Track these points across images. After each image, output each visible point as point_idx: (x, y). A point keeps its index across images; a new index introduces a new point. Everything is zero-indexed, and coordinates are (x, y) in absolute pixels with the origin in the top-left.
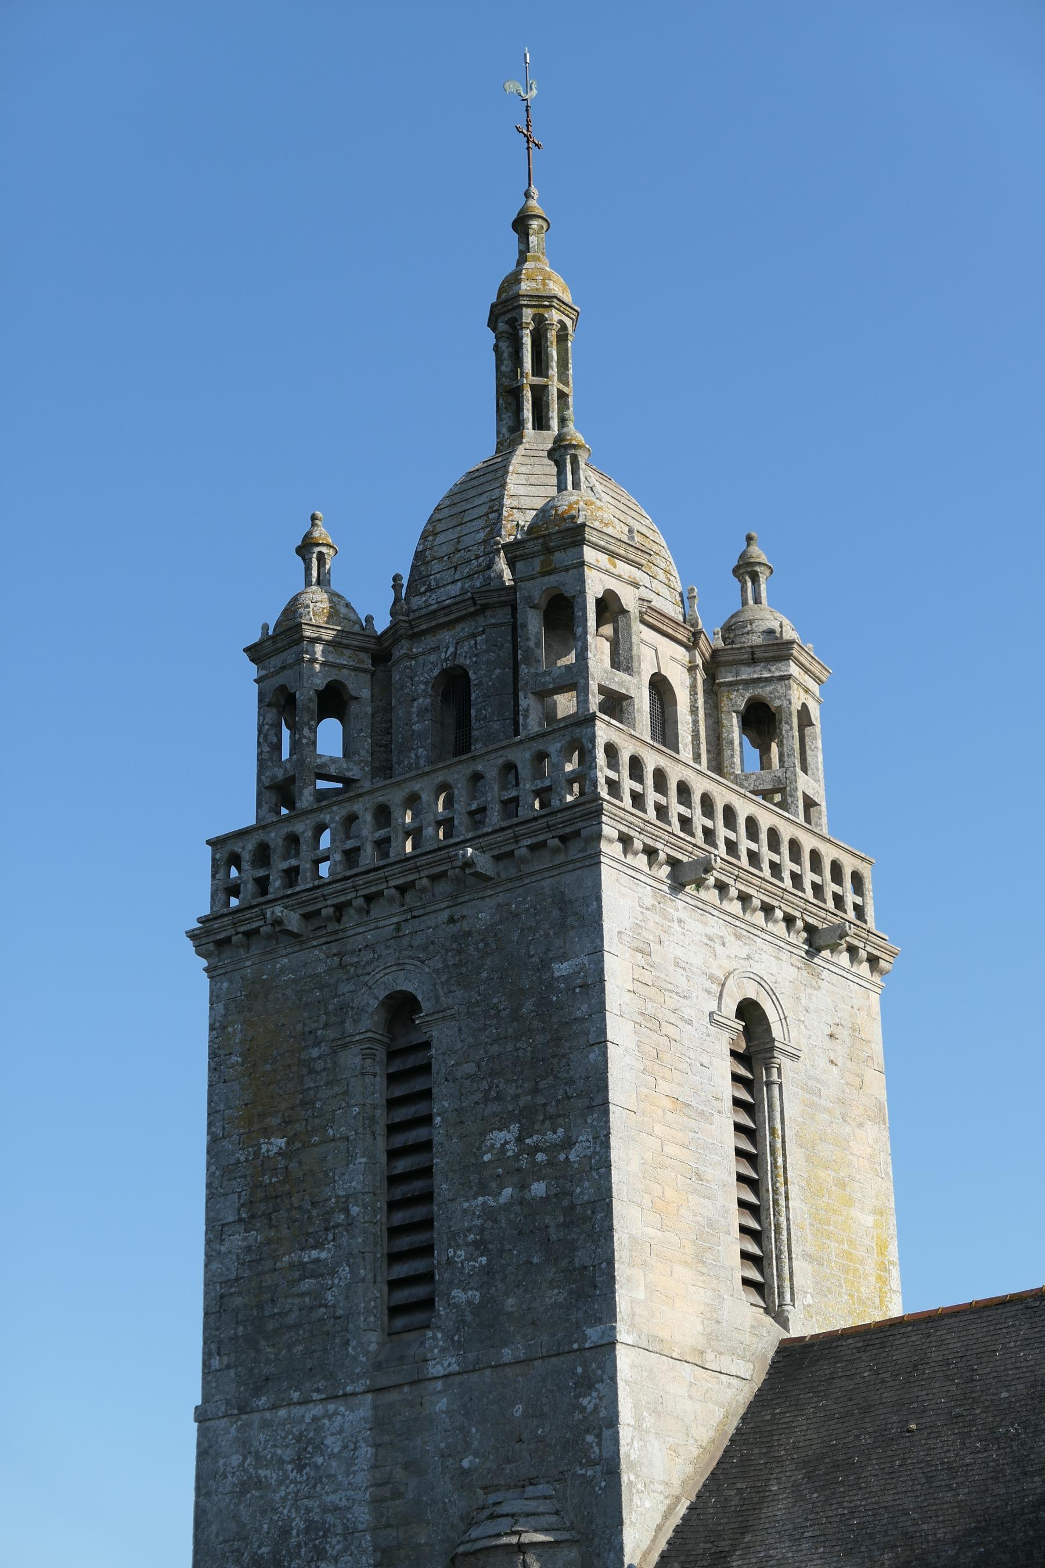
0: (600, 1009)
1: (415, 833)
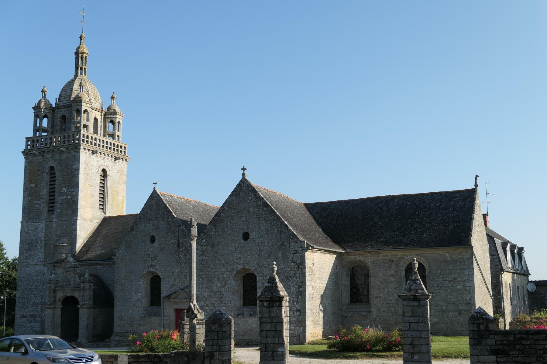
0: (79, 173)
1: (55, 142)
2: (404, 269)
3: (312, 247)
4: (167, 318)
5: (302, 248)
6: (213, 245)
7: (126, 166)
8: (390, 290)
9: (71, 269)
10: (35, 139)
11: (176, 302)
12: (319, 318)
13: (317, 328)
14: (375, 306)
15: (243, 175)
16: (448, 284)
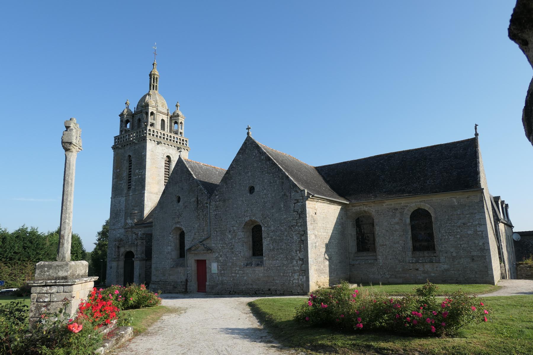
2: (409, 217)
3: (313, 196)
4: (190, 268)
5: (303, 197)
6: (224, 201)
7: (187, 154)
8: (395, 238)
9: (129, 229)
10: (122, 136)
11: (196, 254)
12: (325, 266)
13: (322, 277)
14: (381, 254)
15: (248, 133)
16: (457, 229)
